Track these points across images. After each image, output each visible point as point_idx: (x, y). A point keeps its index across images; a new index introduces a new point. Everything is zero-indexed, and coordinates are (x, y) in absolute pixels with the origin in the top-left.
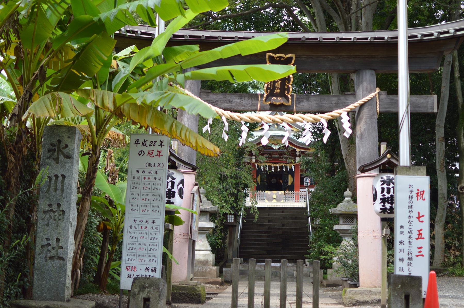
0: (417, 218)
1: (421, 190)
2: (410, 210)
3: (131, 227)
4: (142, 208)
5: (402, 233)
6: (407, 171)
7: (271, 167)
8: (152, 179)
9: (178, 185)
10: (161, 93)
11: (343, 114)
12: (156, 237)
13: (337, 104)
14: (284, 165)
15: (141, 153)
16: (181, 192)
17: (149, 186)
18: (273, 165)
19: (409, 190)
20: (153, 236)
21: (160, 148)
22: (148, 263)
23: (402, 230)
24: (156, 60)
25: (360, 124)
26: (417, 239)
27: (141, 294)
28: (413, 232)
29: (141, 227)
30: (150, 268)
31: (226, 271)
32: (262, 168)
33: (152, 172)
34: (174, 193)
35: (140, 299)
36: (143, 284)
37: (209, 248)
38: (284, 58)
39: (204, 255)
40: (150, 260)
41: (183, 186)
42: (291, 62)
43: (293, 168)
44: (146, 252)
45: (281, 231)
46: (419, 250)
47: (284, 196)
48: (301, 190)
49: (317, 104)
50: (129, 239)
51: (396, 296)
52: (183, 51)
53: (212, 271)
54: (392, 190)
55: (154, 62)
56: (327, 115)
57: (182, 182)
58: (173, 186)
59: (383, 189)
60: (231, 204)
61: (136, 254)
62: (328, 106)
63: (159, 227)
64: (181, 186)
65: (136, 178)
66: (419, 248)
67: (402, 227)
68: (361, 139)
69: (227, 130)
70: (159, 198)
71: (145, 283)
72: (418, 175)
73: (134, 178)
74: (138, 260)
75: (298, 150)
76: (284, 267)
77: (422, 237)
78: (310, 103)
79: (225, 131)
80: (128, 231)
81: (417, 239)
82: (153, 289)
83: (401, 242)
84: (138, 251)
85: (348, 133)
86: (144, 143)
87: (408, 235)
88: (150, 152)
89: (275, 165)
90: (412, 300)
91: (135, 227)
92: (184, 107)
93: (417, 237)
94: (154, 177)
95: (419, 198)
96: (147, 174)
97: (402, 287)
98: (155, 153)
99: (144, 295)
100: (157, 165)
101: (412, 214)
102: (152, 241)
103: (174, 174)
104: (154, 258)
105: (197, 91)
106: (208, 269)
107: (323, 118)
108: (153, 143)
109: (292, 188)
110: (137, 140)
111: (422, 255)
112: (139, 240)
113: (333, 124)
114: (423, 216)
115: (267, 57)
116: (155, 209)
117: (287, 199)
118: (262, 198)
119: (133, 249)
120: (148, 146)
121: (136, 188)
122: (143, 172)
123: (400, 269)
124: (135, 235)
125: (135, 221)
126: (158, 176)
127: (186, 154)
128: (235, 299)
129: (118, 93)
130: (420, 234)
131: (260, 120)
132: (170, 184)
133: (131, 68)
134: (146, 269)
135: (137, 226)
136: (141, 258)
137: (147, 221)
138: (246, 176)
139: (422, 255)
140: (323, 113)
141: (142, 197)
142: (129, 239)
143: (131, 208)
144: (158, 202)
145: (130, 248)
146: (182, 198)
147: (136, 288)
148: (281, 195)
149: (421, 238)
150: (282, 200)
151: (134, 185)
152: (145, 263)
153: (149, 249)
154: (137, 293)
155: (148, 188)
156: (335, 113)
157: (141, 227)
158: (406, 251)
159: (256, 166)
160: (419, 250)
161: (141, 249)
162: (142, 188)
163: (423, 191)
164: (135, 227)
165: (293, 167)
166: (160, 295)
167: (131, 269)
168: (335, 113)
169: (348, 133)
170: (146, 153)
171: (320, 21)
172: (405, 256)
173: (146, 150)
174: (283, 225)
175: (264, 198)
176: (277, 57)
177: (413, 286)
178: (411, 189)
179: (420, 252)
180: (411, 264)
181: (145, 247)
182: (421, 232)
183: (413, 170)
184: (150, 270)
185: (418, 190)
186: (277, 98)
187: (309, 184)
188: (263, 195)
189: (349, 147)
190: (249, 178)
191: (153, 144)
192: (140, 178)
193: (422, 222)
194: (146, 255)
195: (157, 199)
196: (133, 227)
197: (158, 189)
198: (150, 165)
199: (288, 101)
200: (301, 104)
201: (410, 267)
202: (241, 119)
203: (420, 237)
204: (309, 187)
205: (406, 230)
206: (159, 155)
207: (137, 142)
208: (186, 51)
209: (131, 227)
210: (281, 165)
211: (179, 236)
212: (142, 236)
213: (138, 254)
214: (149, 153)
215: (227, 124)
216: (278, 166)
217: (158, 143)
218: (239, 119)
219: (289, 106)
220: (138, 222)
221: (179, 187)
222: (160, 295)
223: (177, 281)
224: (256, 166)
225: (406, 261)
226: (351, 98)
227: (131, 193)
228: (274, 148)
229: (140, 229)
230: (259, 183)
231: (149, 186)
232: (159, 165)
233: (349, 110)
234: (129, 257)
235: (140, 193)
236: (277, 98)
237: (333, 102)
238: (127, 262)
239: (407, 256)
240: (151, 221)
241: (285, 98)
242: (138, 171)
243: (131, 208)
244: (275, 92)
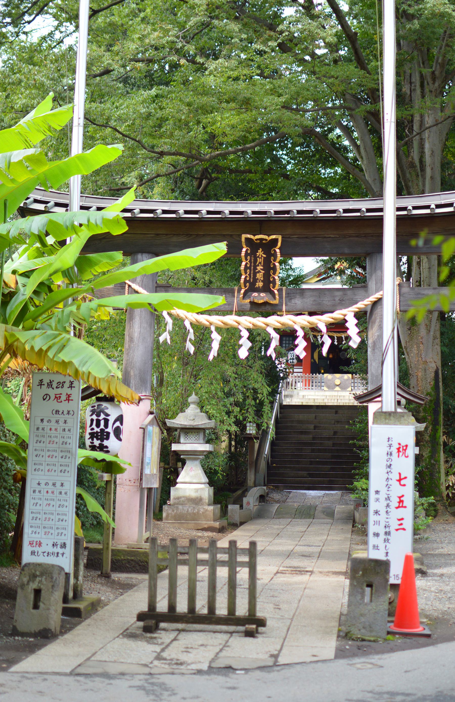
0: (397, 480)
1: (403, 444)
2: (389, 470)
3: (34, 491)
4: (47, 468)
5: (377, 500)
6: (386, 419)
7: (334, 337)
8: (60, 430)
9: (114, 424)
10: (54, 334)
11: (348, 314)
12: (66, 504)
13: (341, 300)
15: (46, 397)
16: (118, 433)
17: (56, 440)
19: (387, 444)
20: (62, 503)
21: (69, 391)
22: (56, 537)
23: (377, 496)
24: (66, 273)
25: (372, 328)
26: (397, 508)
27: (31, 584)
28: (391, 499)
29: (47, 492)
30: (59, 543)
31: (232, 510)
33: (60, 422)
34: (108, 433)
35: (29, 591)
36: (33, 571)
37: (205, 479)
38: (266, 240)
39: (197, 490)
40: (58, 533)
41: (122, 424)
42: (277, 245)
44: (53, 523)
45: (330, 443)
46: (400, 522)
47: (353, 381)
49: (314, 300)
50: (32, 507)
51: (355, 586)
52: (100, 261)
53: (208, 513)
54: (102, 423)
55: (63, 277)
56: (327, 318)
57: (120, 419)
58: (106, 426)
59: (92, 420)
60: (235, 417)
61: (40, 525)
62: (330, 303)
63: (68, 491)
64: (118, 424)
65: (40, 429)
66: (399, 520)
67: (377, 492)
68: (374, 350)
69: (193, 338)
70: (68, 455)
71: (35, 571)
72: (401, 424)
73: (38, 429)
74: (43, 533)
76: (212, 549)
77: (404, 505)
78: (305, 300)
79: (190, 340)
80: (31, 497)
81: (397, 508)
82: (46, 579)
83: (376, 512)
84: (44, 522)
85: (355, 342)
86: (50, 385)
87: (385, 503)
88: (57, 396)
89: (339, 335)
90: (376, 591)
91: (40, 492)
92: (73, 361)
93: (397, 505)
94: (62, 428)
95: (401, 454)
96: (53, 424)
97: (363, 575)
98: (64, 397)
99: (34, 585)
100: (65, 412)
101: (391, 476)
102: (61, 509)
103: (107, 408)
104: (63, 531)
105: (151, 286)
106: (202, 510)
107: (321, 322)
108: (61, 385)
110: (41, 381)
111: (404, 529)
112: (45, 508)
113: (339, 327)
114: (406, 478)
115: (243, 240)
116: (63, 468)
117: (356, 385)
118: (319, 384)
119: (38, 519)
120: (55, 388)
121: (40, 442)
122: (49, 421)
123: (374, 546)
124: (40, 502)
125: (39, 484)
126: (67, 427)
127: (137, 372)
128: (153, 588)
129: (13, 325)
130: (401, 501)
131: (237, 324)
132: (102, 423)
133: (32, 284)
134: (53, 545)
135: (42, 490)
136: (47, 530)
137: (54, 484)
138: (255, 377)
139: (404, 529)
140: (322, 313)
141: (48, 454)
142: (32, 507)
143: (34, 467)
144: (67, 460)
145: (33, 517)
146: (120, 440)
147: (25, 577)
148: (347, 380)
149: (402, 507)
151: (37, 438)
152: (52, 537)
153: (57, 520)
154: (26, 583)
155: (55, 442)
156: (338, 315)
157: (47, 492)
158: (383, 524)
160: (400, 522)
161: (47, 519)
162: (48, 442)
163: (407, 446)
164: (40, 492)
166: (53, 586)
167: (34, 544)
168: (338, 315)
169: (355, 342)
170: (53, 397)
171: (365, 149)
172: (381, 530)
173: (52, 392)
174: (335, 433)
175: (323, 384)
176: (256, 240)
177: (378, 573)
178: (390, 442)
179: (401, 524)
180: (388, 540)
181: (52, 517)
182: (402, 499)
183: (394, 417)
184: (59, 546)
185: (399, 444)
186: (259, 295)
188: (321, 379)
189: (409, 329)
190: (260, 379)
191: (61, 385)
192: (45, 429)
193: (404, 485)
194: (53, 526)
195: (66, 456)
196: (37, 492)
197: (68, 443)
198: (57, 412)
199: (275, 298)
200: (293, 301)
201: (387, 544)
202: (211, 324)
203: (401, 505)
205: (382, 496)
206: (69, 400)
207: (41, 383)
208: (105, 261)
209: (34, 491)
211: (128, 483)
212: (48, 502)
213: (43, 526)
214: (56, 397)
215: (192, 331)
216: (343, 336)
217: (67, 384)
218: (208, 323)
219: (276, 305)
220: (43, 485)
221: (115, 426)
222: (53, 586)
223: (126, 542)
225: (382, 537)
226: (361, 292)
227: (34, 448)
229: (45, 494)
230: (317, 361)
231: (56, 440)
232: (68, 413)
233: (357, 310)
234: (33, 529)
235: (45, 449)
236: (259, 295)
237: (337, 299)
238: (30, 535)
239: (384, 530)
240: (58, 484)
241: (271, 293)
242: (42, 420)
243: (34, 467)
244: (257, 286)
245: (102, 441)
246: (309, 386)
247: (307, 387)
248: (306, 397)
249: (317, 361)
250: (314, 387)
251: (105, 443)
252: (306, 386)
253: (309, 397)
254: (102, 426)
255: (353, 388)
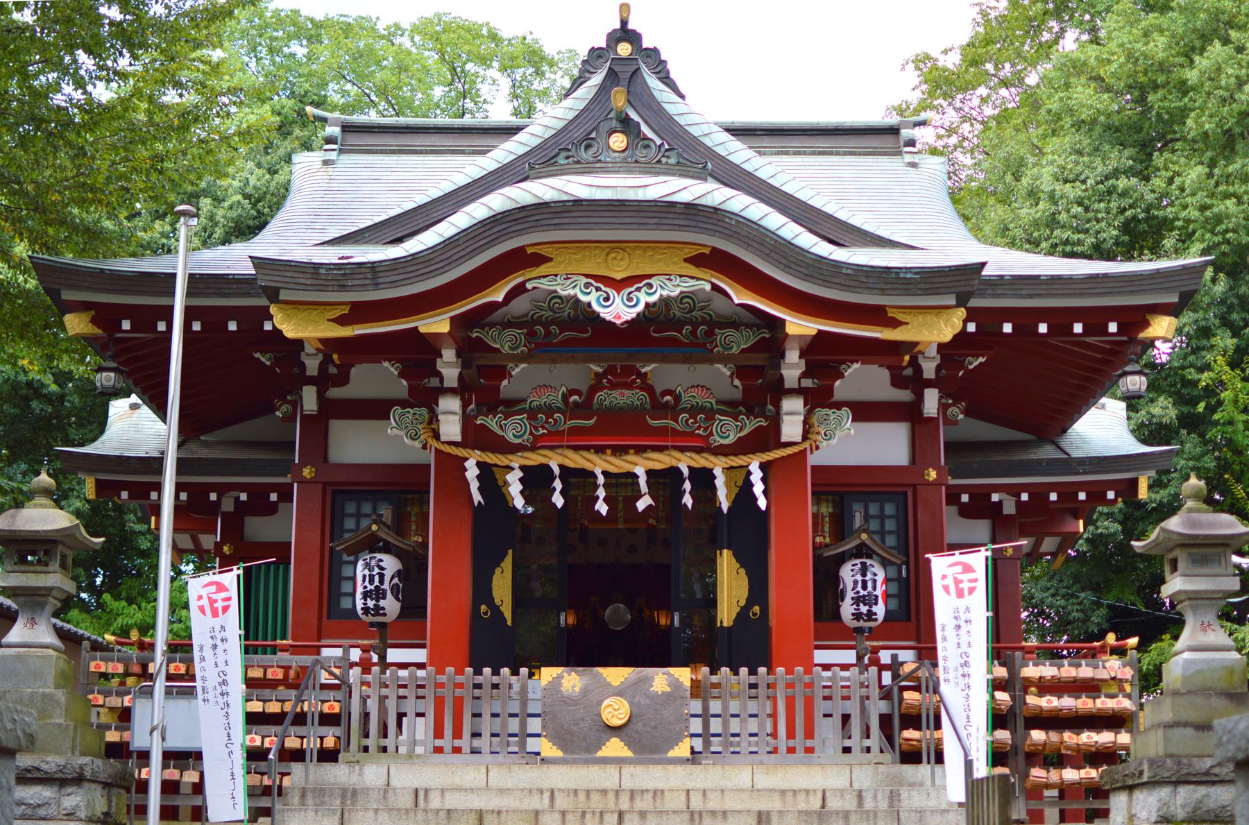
14: (684, 463)
18: (600, 465)
32: (515, 489)
34: (385, 591)
43: (758, 488)
48: (821, 656)
58: (382, 581)
59: (856, 582)
75: (799, 326)
89: (618, 465)
109: (747, 646)
132: (377, 578)
150: (676, 740)
159: (472, 472)
165: (756, 476)
187: (880, 610)
204: (874, 634)
210: (661, 461)
216: (640, 471)
224: (472, 472)
228: (607, 314)
230: (508, 615)
245: (378, 601)
246: (457, 734)
247: (447, 742)
248: (435, 803)
249: (508, 615)
250: (483, 743)
251: (382, 603)
252: (439, 734)
253: (452, 801)
254: (377, 582)
255: (698, 744)
